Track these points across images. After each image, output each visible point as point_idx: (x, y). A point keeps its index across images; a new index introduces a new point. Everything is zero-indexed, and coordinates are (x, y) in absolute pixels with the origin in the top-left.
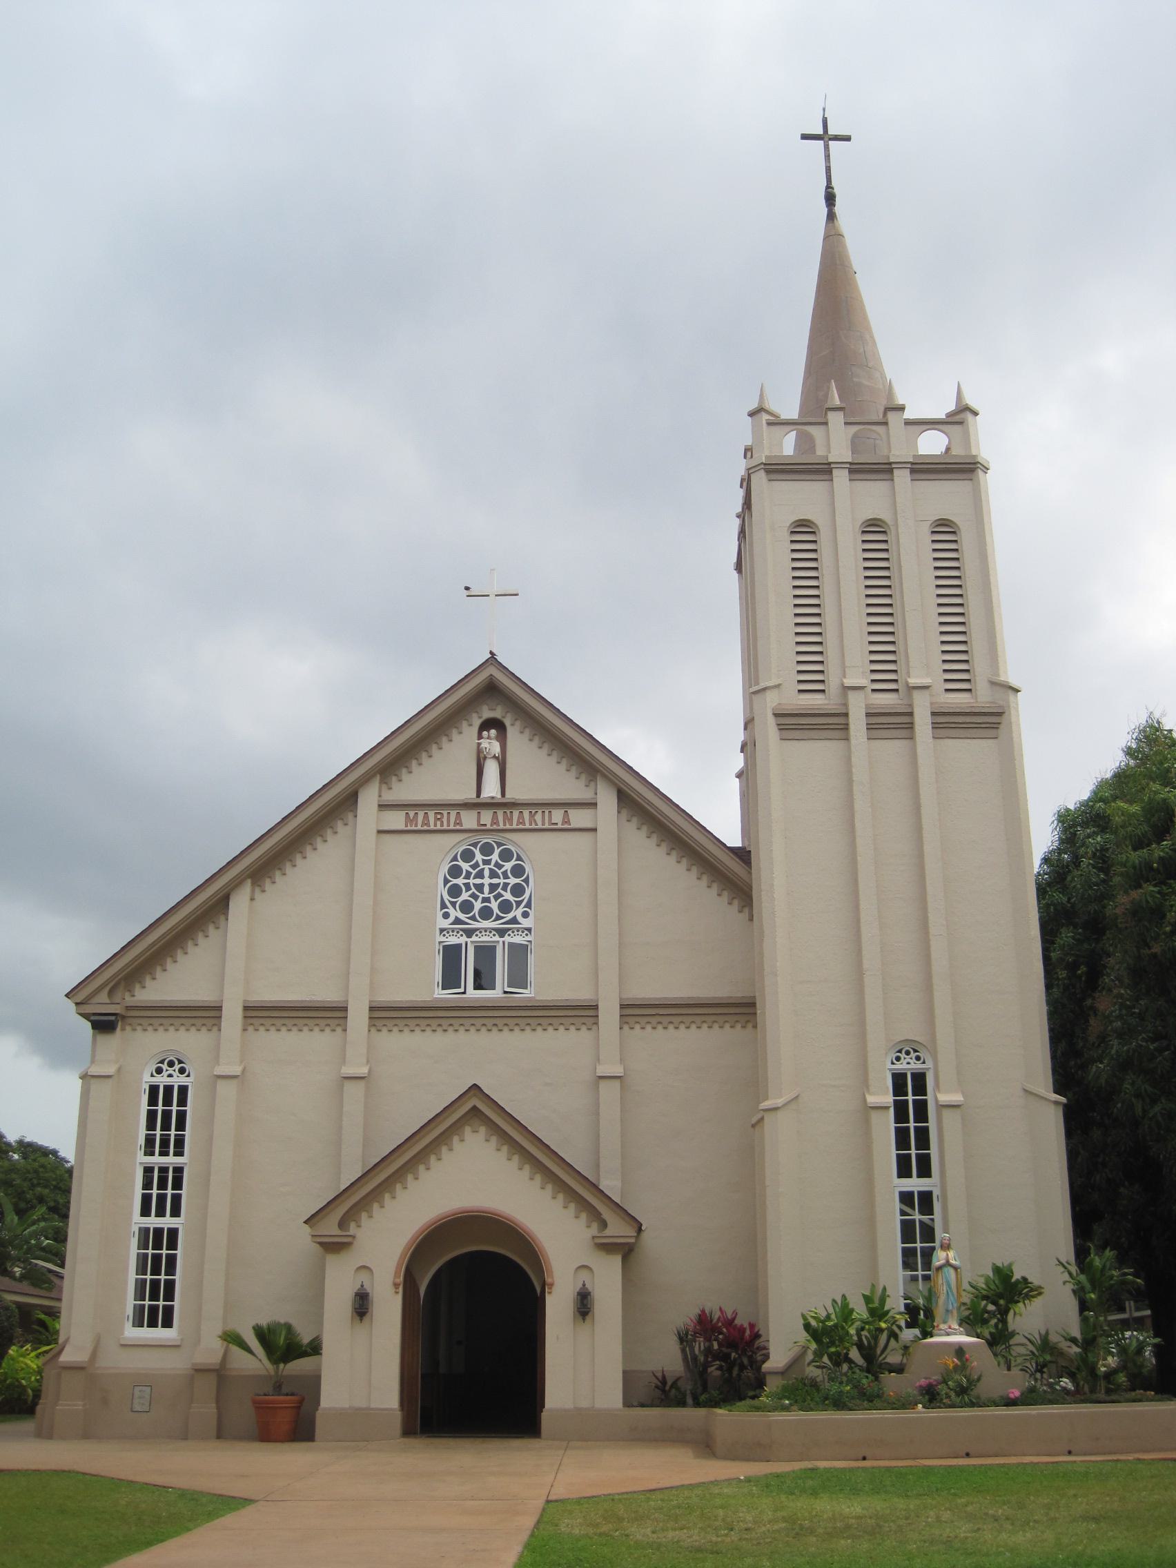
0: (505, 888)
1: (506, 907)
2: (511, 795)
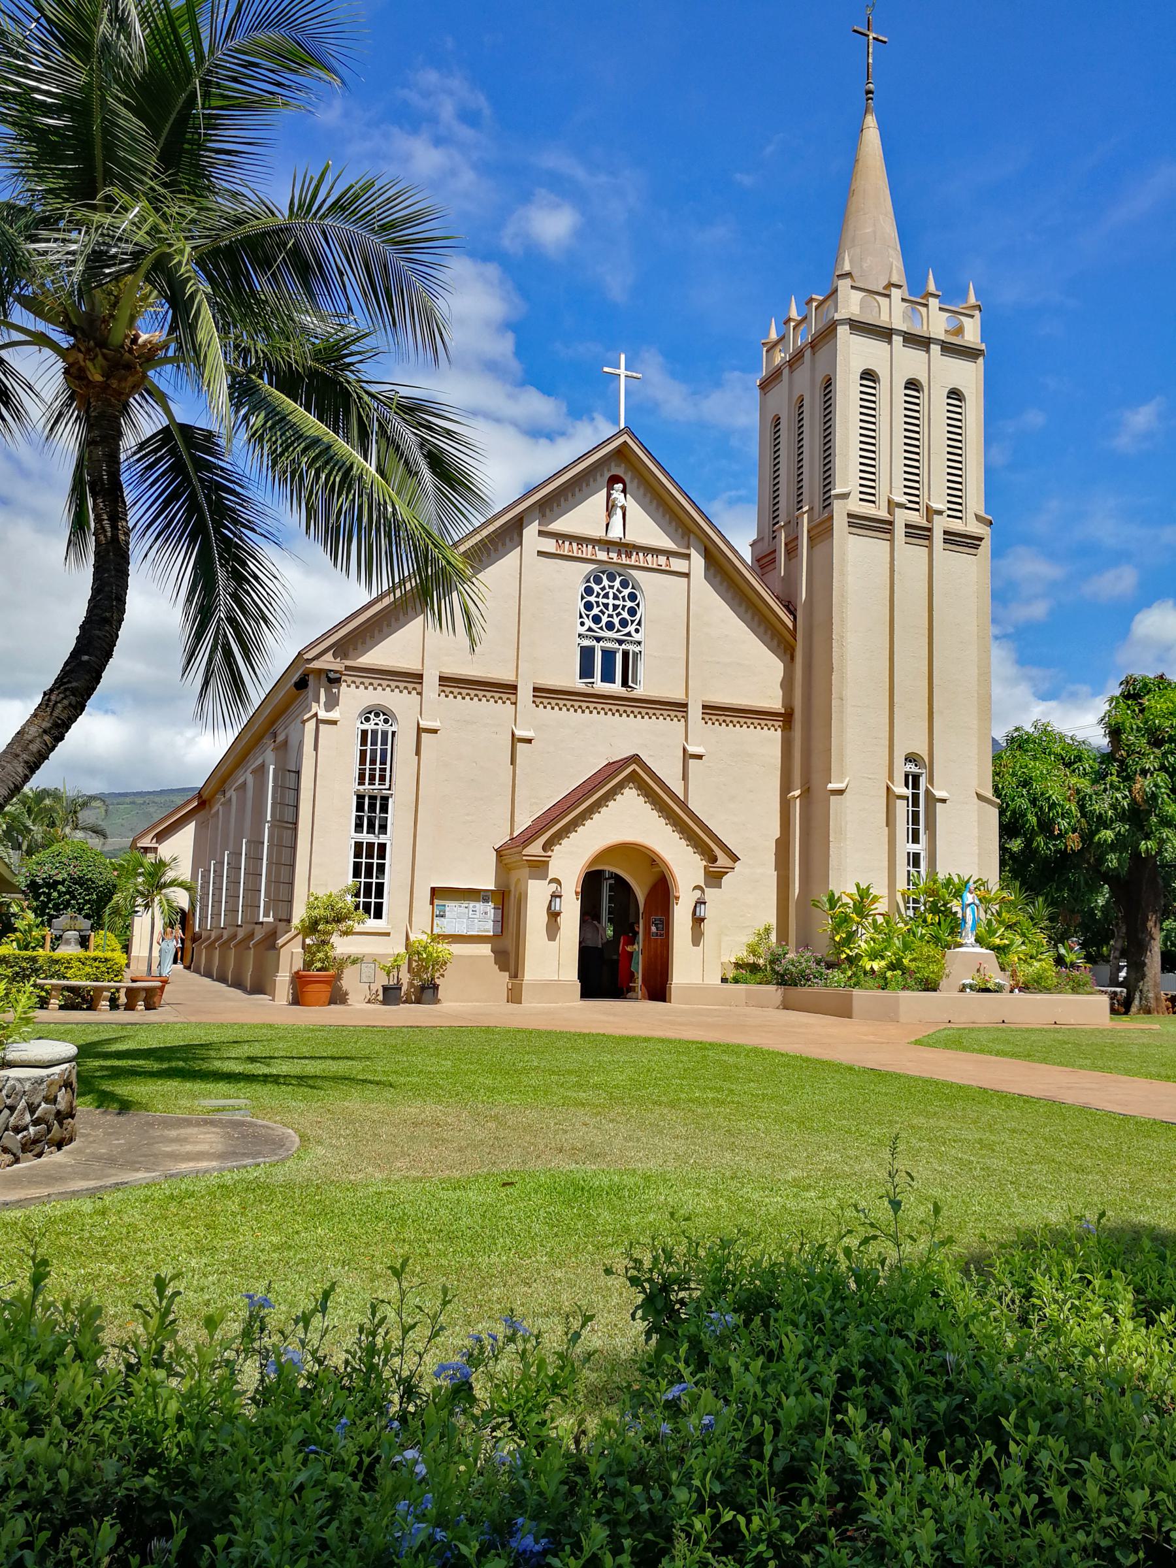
0: (623, 609)
1: (624, 623)
2: (630, 538)
